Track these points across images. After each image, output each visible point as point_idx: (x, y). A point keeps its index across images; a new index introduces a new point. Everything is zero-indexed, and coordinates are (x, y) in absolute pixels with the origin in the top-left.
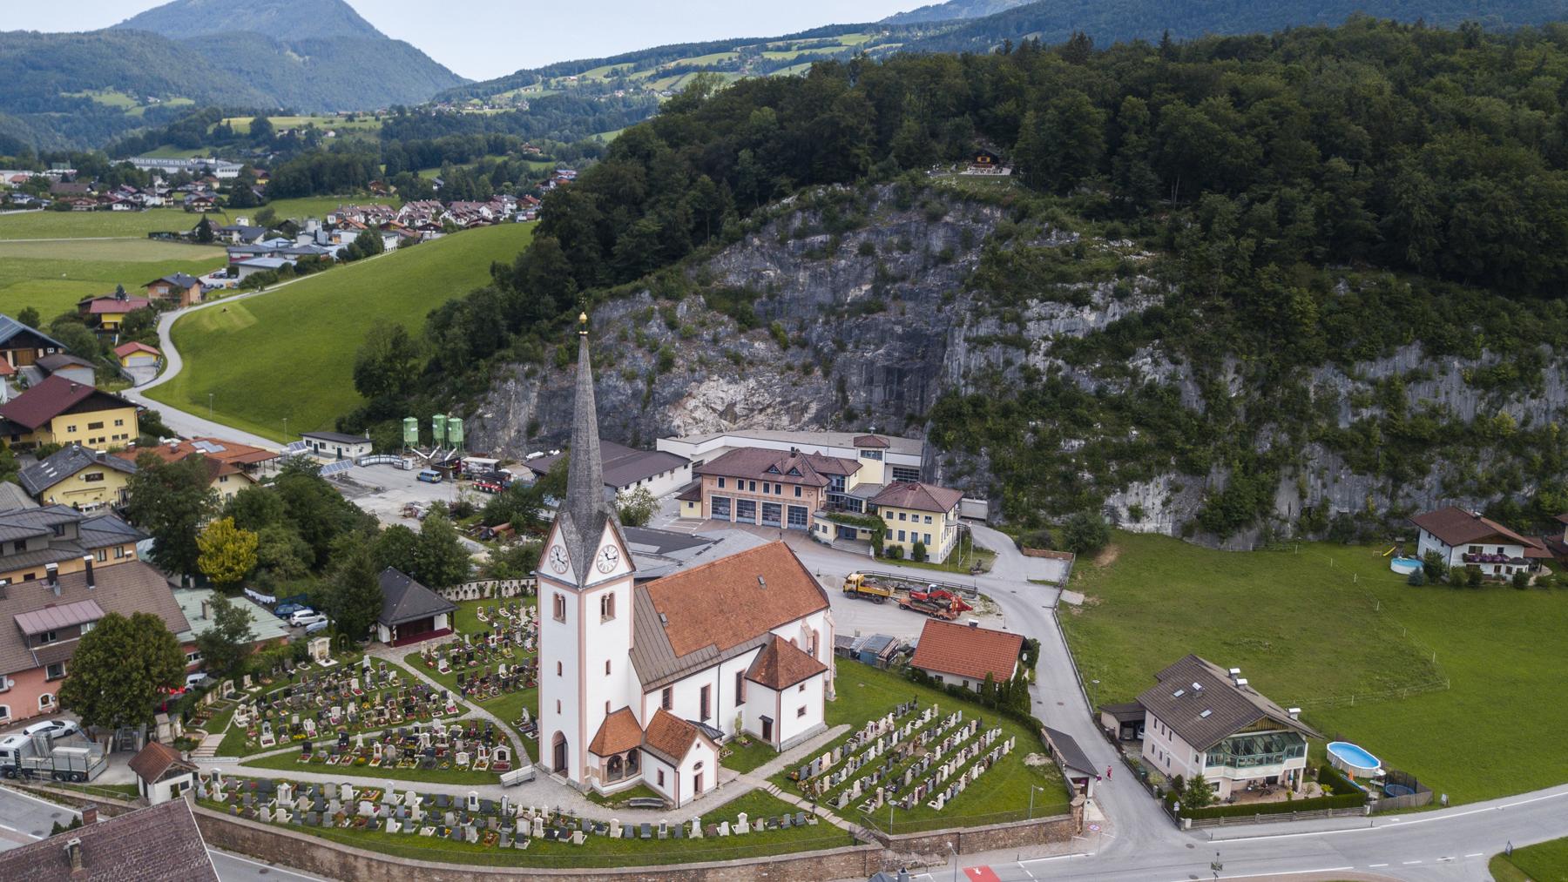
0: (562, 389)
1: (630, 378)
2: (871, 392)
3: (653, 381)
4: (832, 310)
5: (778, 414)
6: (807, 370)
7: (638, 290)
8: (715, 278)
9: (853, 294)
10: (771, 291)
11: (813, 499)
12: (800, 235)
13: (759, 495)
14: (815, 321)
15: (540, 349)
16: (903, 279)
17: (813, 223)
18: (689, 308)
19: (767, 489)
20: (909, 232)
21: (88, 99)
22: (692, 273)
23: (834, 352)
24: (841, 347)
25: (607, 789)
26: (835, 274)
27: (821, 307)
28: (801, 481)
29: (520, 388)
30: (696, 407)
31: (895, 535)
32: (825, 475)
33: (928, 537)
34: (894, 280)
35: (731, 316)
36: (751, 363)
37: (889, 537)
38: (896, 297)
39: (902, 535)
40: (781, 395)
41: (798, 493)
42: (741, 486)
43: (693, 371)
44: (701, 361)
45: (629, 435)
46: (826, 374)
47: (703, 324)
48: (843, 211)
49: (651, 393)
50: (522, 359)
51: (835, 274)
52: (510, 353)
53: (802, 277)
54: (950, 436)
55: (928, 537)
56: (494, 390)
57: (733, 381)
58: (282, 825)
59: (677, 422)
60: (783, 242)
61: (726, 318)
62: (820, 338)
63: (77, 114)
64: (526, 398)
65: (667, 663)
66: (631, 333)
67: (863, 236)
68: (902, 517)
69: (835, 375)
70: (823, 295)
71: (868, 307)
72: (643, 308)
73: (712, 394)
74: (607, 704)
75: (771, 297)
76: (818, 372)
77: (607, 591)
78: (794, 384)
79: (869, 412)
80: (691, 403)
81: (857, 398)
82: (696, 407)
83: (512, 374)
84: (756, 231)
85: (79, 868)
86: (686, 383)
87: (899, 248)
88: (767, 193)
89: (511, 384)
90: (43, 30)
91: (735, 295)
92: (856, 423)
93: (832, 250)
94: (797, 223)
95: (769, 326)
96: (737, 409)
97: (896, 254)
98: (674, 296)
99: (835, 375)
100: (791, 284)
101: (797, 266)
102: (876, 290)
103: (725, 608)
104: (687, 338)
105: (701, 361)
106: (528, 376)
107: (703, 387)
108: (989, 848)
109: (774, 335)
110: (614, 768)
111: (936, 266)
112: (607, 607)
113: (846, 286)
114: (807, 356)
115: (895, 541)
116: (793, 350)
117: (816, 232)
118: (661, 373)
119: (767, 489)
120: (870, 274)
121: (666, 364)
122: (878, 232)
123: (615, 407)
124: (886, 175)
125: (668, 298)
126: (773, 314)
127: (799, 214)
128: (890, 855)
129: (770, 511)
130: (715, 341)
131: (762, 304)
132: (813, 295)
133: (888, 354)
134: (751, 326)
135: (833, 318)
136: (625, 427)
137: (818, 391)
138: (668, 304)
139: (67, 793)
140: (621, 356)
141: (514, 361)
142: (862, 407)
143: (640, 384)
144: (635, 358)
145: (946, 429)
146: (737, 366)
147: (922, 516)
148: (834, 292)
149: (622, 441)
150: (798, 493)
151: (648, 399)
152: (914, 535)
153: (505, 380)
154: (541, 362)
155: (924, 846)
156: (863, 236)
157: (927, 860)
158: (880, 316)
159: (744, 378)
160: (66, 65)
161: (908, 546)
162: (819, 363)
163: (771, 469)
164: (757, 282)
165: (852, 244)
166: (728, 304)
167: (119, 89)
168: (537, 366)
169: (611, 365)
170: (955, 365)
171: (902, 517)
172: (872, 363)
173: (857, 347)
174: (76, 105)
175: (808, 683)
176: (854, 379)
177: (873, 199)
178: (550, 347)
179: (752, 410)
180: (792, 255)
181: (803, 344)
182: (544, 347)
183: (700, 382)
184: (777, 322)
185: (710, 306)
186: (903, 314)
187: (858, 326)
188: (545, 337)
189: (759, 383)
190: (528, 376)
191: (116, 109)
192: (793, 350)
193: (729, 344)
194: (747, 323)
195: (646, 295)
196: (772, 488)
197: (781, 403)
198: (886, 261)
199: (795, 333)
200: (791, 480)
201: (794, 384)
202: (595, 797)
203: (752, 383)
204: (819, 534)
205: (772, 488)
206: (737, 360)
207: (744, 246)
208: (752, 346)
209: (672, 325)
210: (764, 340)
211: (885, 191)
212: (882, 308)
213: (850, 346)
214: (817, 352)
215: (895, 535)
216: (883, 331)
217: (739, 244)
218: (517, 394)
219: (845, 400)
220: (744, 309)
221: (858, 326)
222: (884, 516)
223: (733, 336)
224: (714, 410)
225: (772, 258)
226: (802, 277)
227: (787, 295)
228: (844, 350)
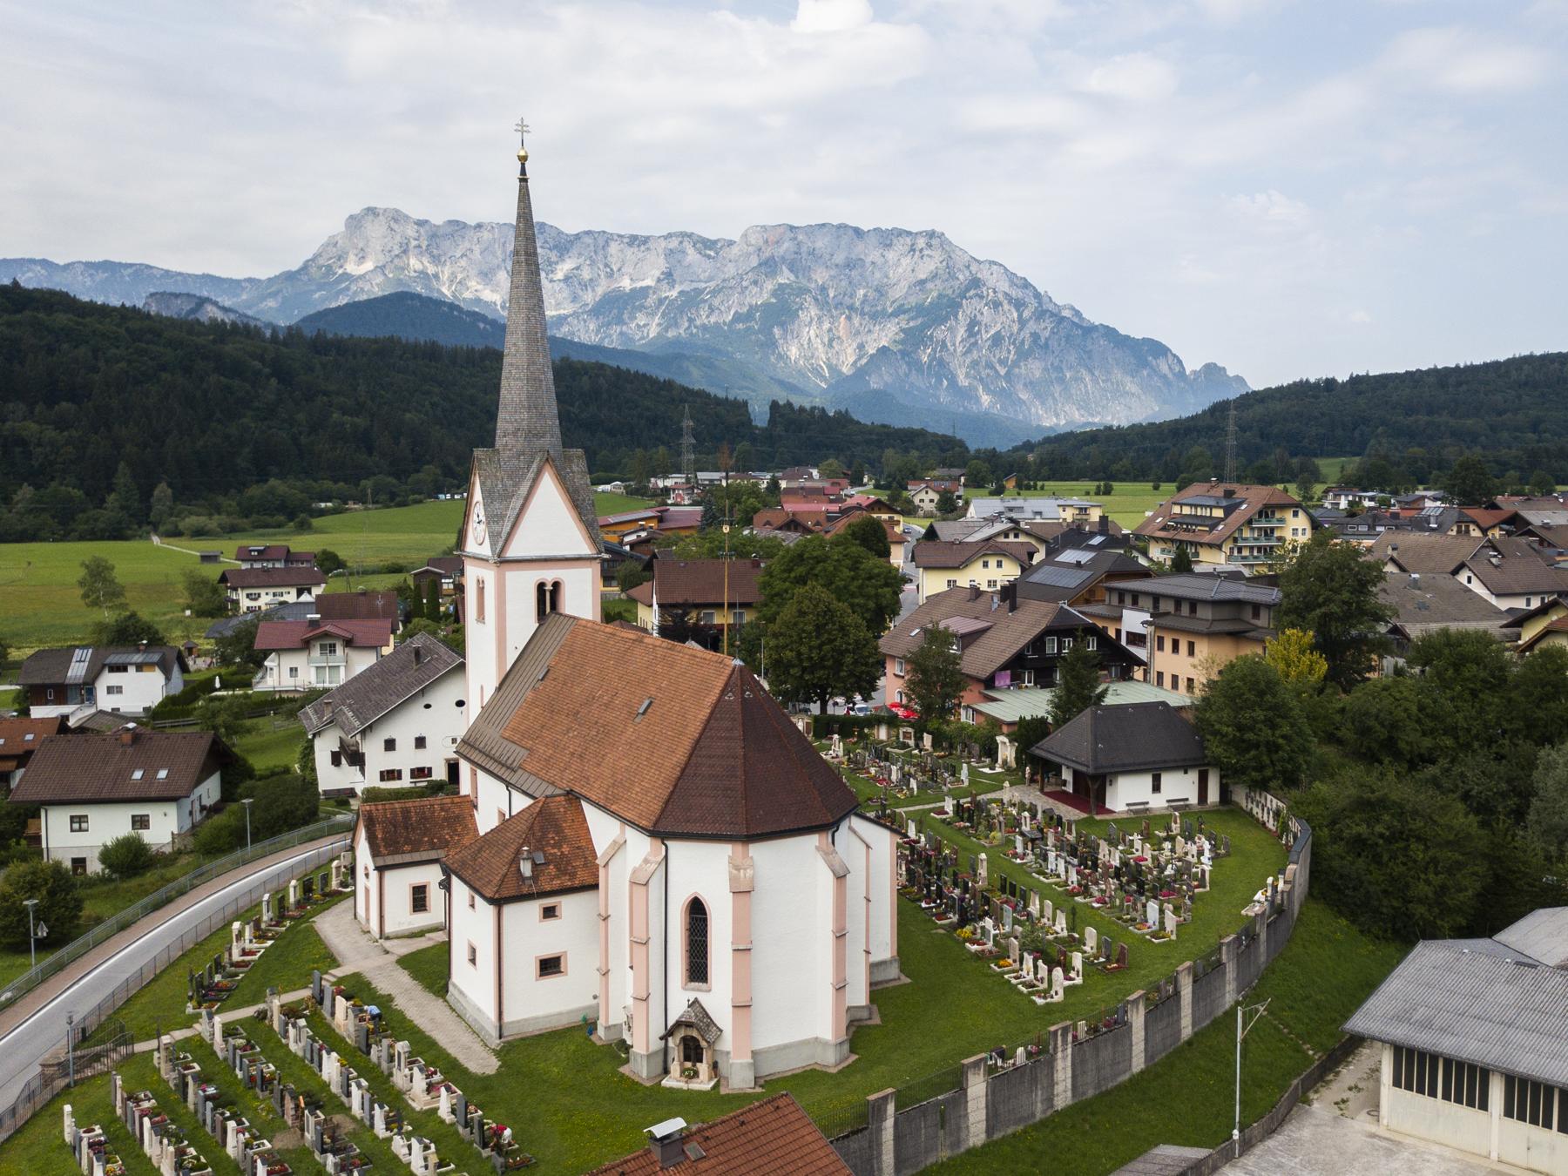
77: (549, 575)
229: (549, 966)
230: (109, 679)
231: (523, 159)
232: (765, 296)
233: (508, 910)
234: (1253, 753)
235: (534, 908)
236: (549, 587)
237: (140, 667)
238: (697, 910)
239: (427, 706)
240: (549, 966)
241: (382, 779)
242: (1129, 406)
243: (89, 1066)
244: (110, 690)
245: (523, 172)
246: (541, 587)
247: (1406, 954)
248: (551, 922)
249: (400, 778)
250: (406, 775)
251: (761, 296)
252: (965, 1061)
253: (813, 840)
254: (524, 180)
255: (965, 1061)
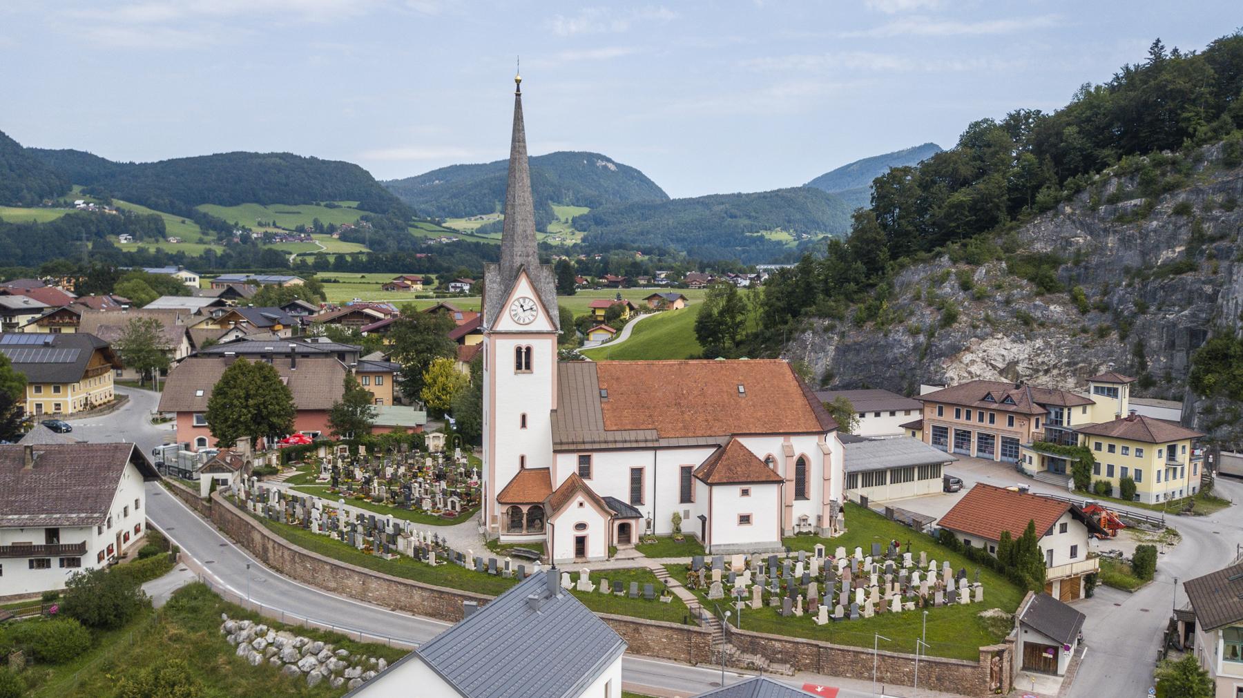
0: (856, 343)
1: (914, 332)
2: (1172, 358)
3: (932, 335)
4: (1139, 274)
5: (1064, 375)
6: (1102, 333)
7: (939, 255)
8: (1019, 246)
9: (1166, 255)
10: (1078, 258)
11: (1024, 430)
12: (1113, 200)
13: (975, 425)
14: (1119, 285)
15: (843, 307)
16: (1222, 237)
17: (1130, 188)
18: (987, 272)
19: (981, 419)
20: (1234, 189)
21: (762, 236)
22: (1000, 241)
23: (1134, 315)
24: (1143, 309)
25: (505, 539)
26: (1145, 236)
27: (1127, 270)
28: (1013, 408)
29: (817, 340)
30: (973, 362)
31: (1104, 470)
32: (1043, 406)
33: (1138, 473)
34: (1212, 239)
35: (1031, 280)
36: (1042, 325)
37: (1098, 472)
38: (1211, 257)
39: (1111, 469)
40: (1069, 356)
41: (1011, 423)
42: (958, 416)
43: (975, 327)
44: (987, 319)
45: (905, 385)
46: (1123, 338)
47: (999, 287)
48: (1164, 174)
49: (929, 346)
50: (822, 315)
51: (1145, 236)
52: (813, 309)
53: (1111, 241)
54: (1210, 379)
55: (1138, 473)
56: (795, 340)
57: (1017, 340)
58: (255, 517)
59: (950, 374)
60: (1094, 209)
61: (1025, 282)
62: (1121, 301)
63: (753, 247)
64: (823, 350)
65: (591, 432)
66: (924, 294)
67: (1182, 197)
68: (1111, 448)
69: (1133, 339)
70: (1132, 258)
71: (1177, 269)
72: (939, 272)
73: (993, 351)
74: (522, 458)
75: (1077, 263)
76: (1114, 335)
77: (524, 343)
78: (1086, 346)
79: (1169, 379)
80: (968, 357)
81: (1157, 364)
82: (973, 362)
83: (811, 327)
84: (1069, 199)
85: (30, 467)
86: (966, 337)
87: (1221, 206)
88: (1092, 164)
89: (809, 335)
90: (744, 191)
91: (1038, 260)
92: (1152, 390)
93: (1147, 212)
94: (1112, 189)
95: (1070, 291)
96: (1020, 368)
97: (1216, 213)
98: (974, 261)
99: (1133, 339)
100: (1099, 250)
101: (1106, 230)
102: (1190, 252)
103: (683, 402)
104: (979, 298)
105: (987, 319)
106: (826, 330)
107: (984, 345)
108: (859, 676)
109: (1075, 299)
110: (515, 522)
111: (1192, 191)
112: (524, 360)
113: (1157, 248)
114: (1106, 320)
115: (1103, 476)
116: (1093, 314)
117: (1130, 196)
118: (942, 327)
119: (981, 419)
120: (1185, 235)
121: (950, 319)
122: (1198, 191)
123: (896, 359)
124: (1216, 135)
125: (968, 263)
126: (1078, 280)
127: (1115, 181)
128: (729, 648)
129: (986, 441)
130: (1007, 302)
131: (1067, 269)
132: (1121, 259)
133: (1193, 315)
134: (1050, 290)
135: (1137, 280)
136: (903, 377)
137: (1111, 353)
138: (966, 267)
139: (176, 483)
140: (912, 313)
141: (814, 315)
142: (1161, 373)
143: (922, 338)
144: (922, 315)
145: (1207, 372)
146: (1025, 325)
147: (1133, 448)
148: (1144, 254)
149: (899, 391)
150: (1011, 423)
151: (925, 352)
152: (1124, 470)
153: (804, 331)
154: (841, 318)
155: (775, 652)
156: (1182, 197)
157: (775, 666)
158: (1189, 277)
159: (1030, 337)
160: (753, 214)
161: (1115, 482)
162: (1118, 327)
163: (987, 397)
164: (1065, 249)
165: (1167, 206)
166: (1031, 270)
167: (785, 229)
168: (837, 323)
169: (901, 322)
170: (1232, 304)
171: (1111, 448)
172: (1174, 325)
173: (1159, 309)
174: (753, 241)
175: (754, 489)
176: (1154, 343)
177: (1199, 160)
178: (853, 307)
179: (1037, 371)
180: (1103, 220)
181: (1103, 308)
182: (847, 307)
183: (983, 339)
184: (1082, 289)
185: (1011, 271)
186: (1215, 273)
187: (1162, 288)
188: (850, 298)
189: (1047, 343)
190: (826, 330)
191: (779, 243)
192: (1093, 314)
193: (1022, 306)
194: (1046, 287)
195: (945, 259)
196: (987, 417)
197: (1068, 364)
198: (1203, 220)
199: (1098, 298)
200: (1003, 407)
201: (1086, 346)
202: (493, 545)
203: (1039, 343)
204: (1026, 466)
205: (987, 417)
206: (1026, 321)
207: (1056, 215)
208: (1047, 309)
209: (966, 286)
210: (1064, 304)
211: (1213, 151)
212: (1192, 268)
213: (1153, 309)
214: (1117, 315)
215: (1104, 470)
216: (1191, 292)
217: (1050, 214)
218: (813, 344)
219: (1143, 366)
220: (1044, 276)
221: (1162, 288)
222: (1092, 447)
223: (1029, 298)
224: (994, 367)
225: (1083, 225)
226: (1111, 241)
227: (1094, 260)
228: (1144, 313)
229: (745, 519)
231: (518, 82)
233: (715, 489)
235: (737, 490)
236: (524, 350)
240: (745, 519)
242: (344, 311)
243: (83, 520)
245: (518, 90)
248: (745, 498)
252: (981, 648)
254: (518, 95)
255: (981, 648)
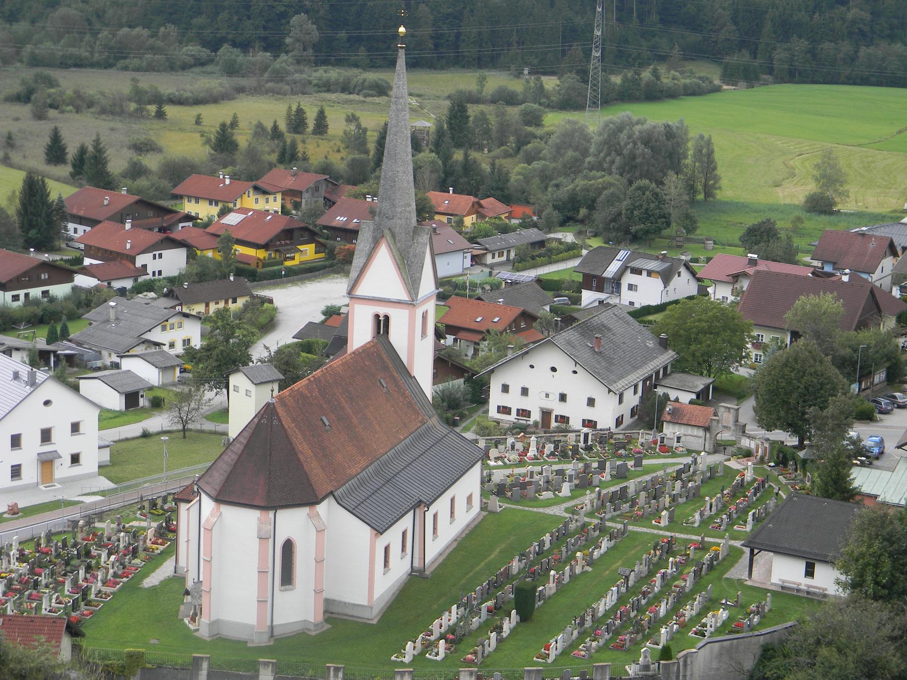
77: (382, 311)
230: (629, 278)
232: (303, 200)
234: (864, 458)
237: (650, 273)
238: (288, 547)
239: (532, 367)
241: (499, 412)
244: (631, 287)
246: (377, 316)
247: (334, 601)
249: (510, 414)
250: (514, 412)
251: (594, 173)
253: (305, 510)
